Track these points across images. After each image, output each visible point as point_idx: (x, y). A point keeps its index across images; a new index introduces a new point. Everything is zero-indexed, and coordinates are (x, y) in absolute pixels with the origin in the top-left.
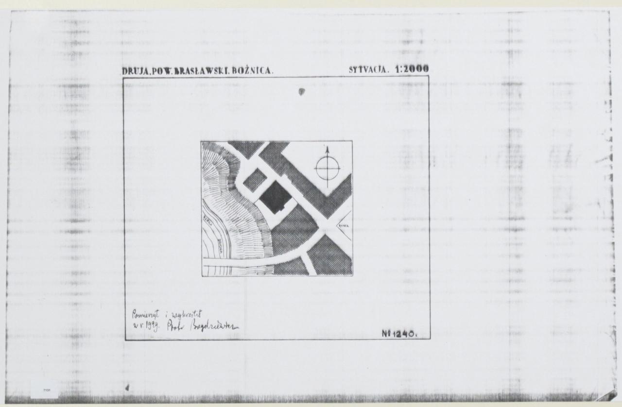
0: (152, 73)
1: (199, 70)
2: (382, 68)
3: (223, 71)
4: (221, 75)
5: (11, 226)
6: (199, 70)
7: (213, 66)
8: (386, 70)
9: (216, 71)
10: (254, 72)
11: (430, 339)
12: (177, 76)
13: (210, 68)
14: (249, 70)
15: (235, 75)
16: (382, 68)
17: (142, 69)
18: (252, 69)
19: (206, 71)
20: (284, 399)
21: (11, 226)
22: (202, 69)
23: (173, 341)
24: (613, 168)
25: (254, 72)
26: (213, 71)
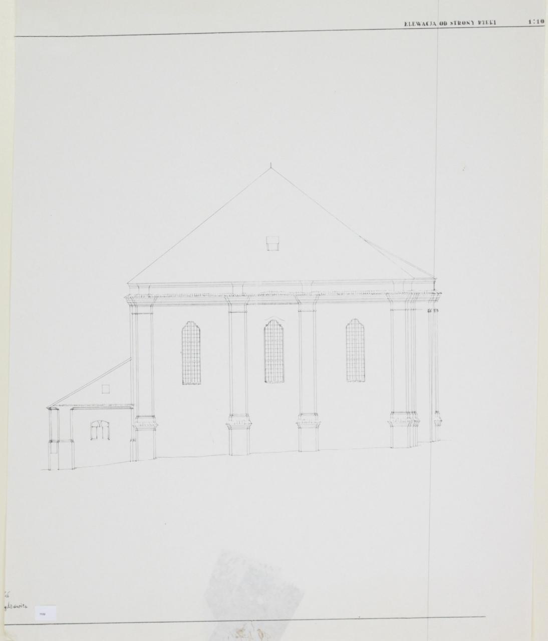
1: (411, 24)
15: (460, 26)
19: (415, 24)
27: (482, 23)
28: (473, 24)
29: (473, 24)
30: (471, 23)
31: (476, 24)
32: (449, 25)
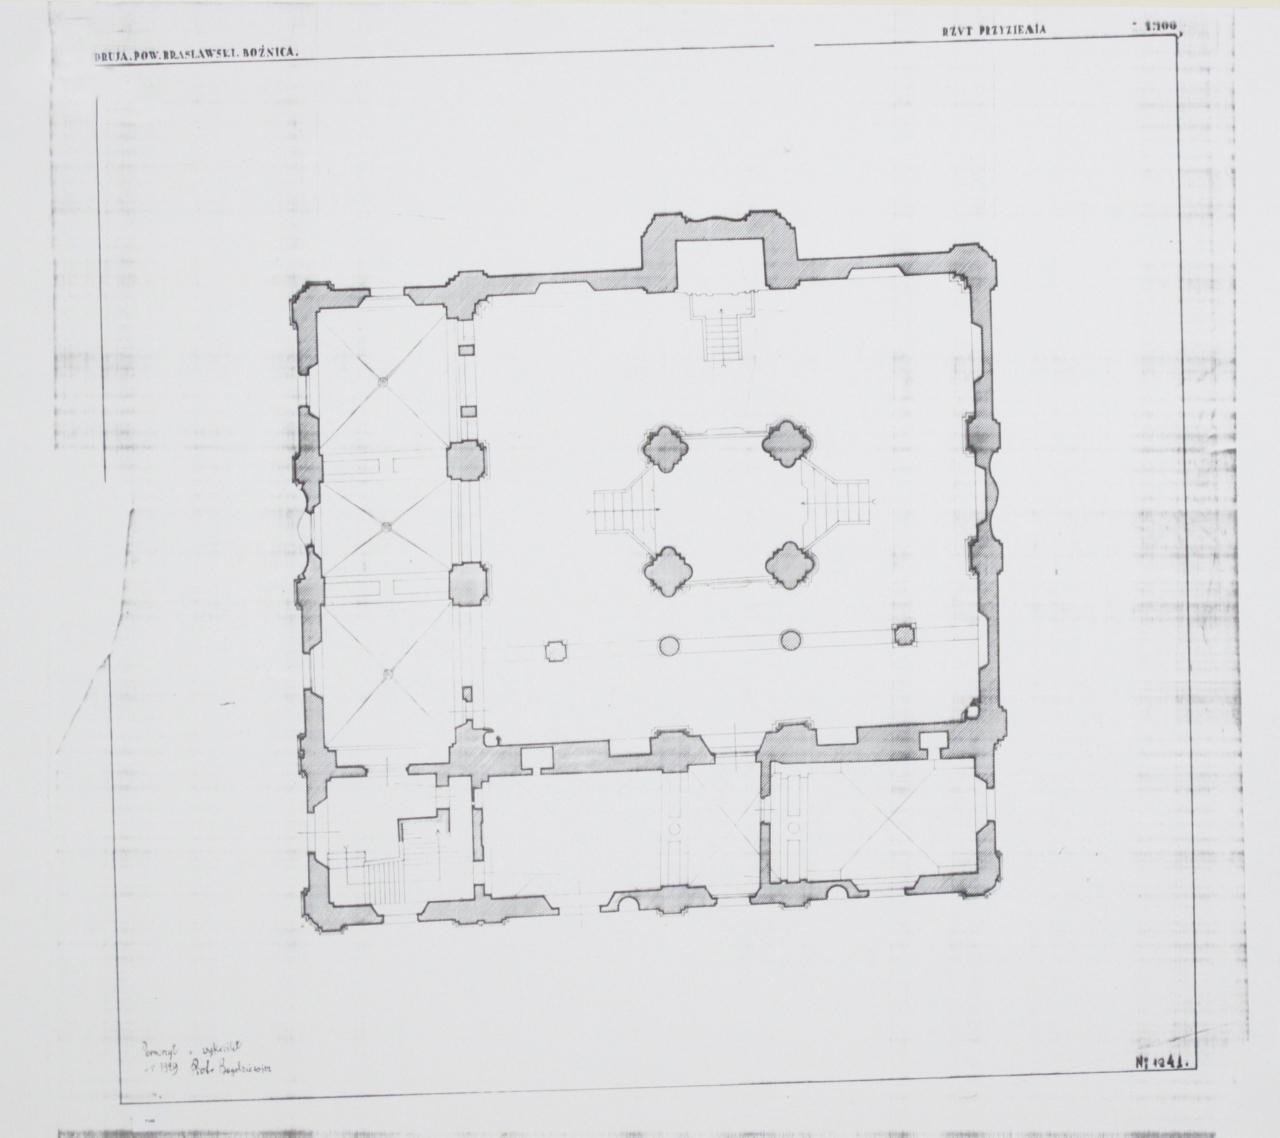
0: (133, 58)
2: (121, 55)
3: (229, 53)
4: (227, 59)
5: (330, 857)
6: (197, 53)
7: (213, 46)
8: (294, 52)
9: (219, 53)
10: (271, 54)
11: (1196, 1068)
12: (246, 59)
13: (210, 51)
14: (266, 52)
16: (121, 55)
17: (118, 54)
18: (269, 51)
20: (805, 430)
21: (330, 857)
22: (201, 52)
23: (618, 268)
24: (130, 509)
25: (271, 54)
26: (215, 54)
27: (950, 32)
28: (969, 34)
29: (969, 34)
30: (965, 32)
31: (975, 33)
32: (975, 33)
